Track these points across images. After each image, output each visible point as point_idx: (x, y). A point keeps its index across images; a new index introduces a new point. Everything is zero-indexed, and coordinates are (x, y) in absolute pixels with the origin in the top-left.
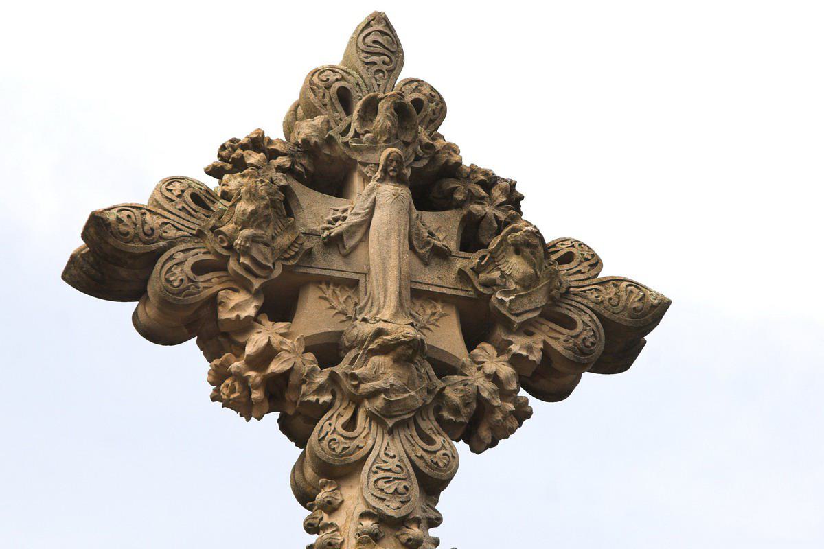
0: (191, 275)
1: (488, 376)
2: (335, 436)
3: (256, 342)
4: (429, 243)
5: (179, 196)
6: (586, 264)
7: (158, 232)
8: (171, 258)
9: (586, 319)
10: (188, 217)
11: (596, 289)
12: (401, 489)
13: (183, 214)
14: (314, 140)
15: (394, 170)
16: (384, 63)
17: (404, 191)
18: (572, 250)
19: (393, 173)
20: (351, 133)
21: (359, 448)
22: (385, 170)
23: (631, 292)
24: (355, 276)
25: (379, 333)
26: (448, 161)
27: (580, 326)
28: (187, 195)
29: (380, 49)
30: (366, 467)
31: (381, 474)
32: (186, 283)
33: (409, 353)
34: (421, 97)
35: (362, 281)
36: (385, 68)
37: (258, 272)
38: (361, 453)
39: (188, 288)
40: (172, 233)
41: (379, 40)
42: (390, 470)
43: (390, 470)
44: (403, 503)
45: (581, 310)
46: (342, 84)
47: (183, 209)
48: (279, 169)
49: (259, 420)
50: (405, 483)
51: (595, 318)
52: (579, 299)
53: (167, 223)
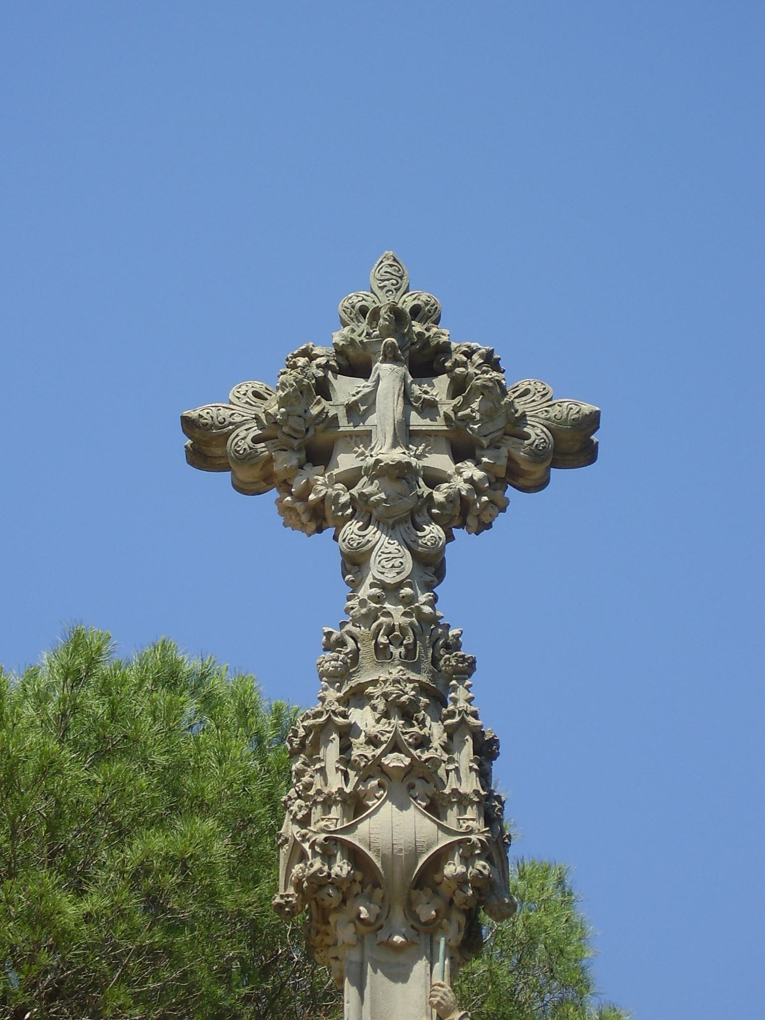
0: (251, 444)
1: (466, 481)
2: (353, 536)
3: (299, 483)
4: (420, 397)
5: (245, 394)
6: (538, 395)
7: (229, 420)
8: (237, 435)
9: (538, 431)
10: (250, 407)
11: (546, 411)
12: (397, 564)
13: (246, 406)
14: (341, 343)
15: (390, 353)
16: (392, 284)
17: (403, 370)
18: (529, 387)
19: (391, 356)
20: (364, 334)
21: (369, 541)
22: (385, 355)
23: (571, 409)
24: (369, 428)
25: (378, 461)
26: (438, 342)
27: (533, 437)
28: (250, 394)
29: (389, 276)
30: (374, 553)
31: (384, 556)
32: (248, 450)
33: (401, 473)
34: (420, 303)
35: (374, 431)
36: (393, 288)
37: (296, 436)
38: (370, 545)
39: (250, 454)
40: (238, 419)
41: (389, 270)
42: (390, 553)
43: (390, 553)
44: (398, 573)
45: (534, 426)
46: (364, 303)
47: (247, 402)
48: (319, 366)
49: (454, 539)
50: (401, 560)
51: (545, 429)
52: (533, 419)
53: (233, 414)
